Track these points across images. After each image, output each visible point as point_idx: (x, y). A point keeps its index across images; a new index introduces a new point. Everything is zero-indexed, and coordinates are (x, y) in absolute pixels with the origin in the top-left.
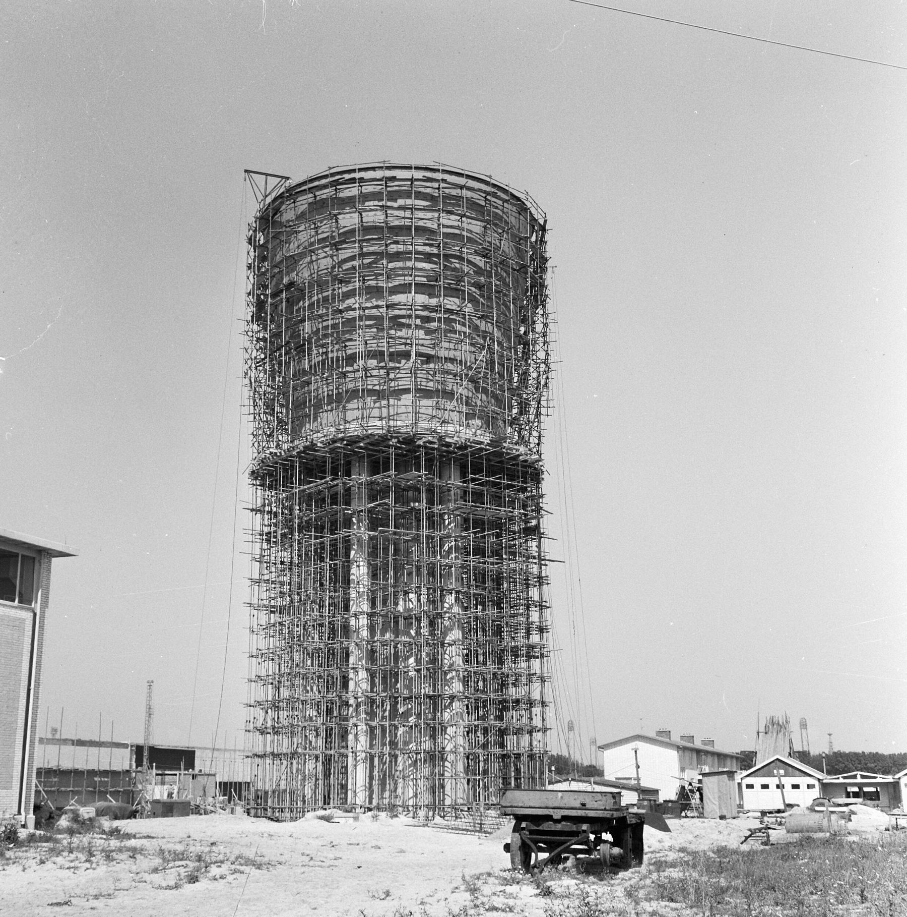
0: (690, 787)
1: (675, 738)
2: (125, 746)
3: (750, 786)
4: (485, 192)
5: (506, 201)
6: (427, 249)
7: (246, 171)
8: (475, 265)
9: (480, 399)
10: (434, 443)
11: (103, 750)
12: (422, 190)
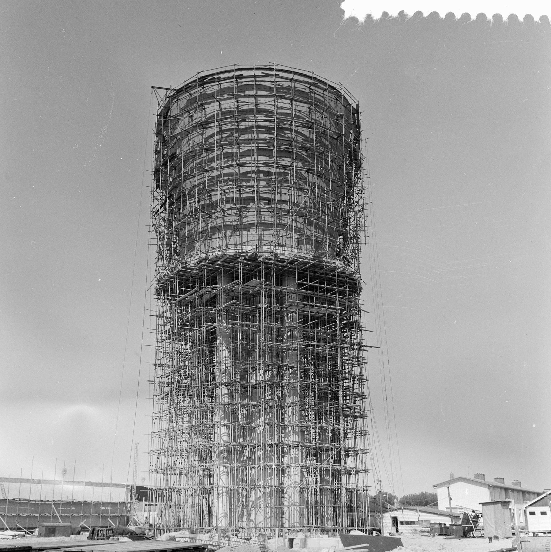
0: (474, 514)
1: (490, 480)
2: (122, 486)
3: (532, 513)
4: (308, 83)
5: (325, 90)
6: (267, 124)
7: (153, 87)
8: (303, 135)
9: (309, 231)
10: (271, 259)
11: (105, 488)
12: (262, 83)
